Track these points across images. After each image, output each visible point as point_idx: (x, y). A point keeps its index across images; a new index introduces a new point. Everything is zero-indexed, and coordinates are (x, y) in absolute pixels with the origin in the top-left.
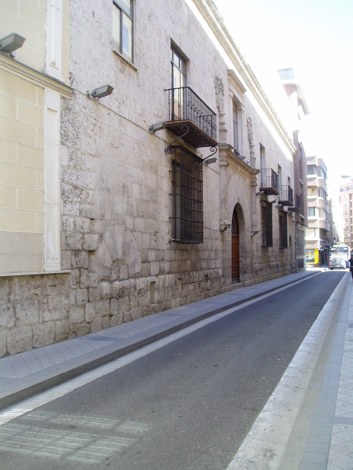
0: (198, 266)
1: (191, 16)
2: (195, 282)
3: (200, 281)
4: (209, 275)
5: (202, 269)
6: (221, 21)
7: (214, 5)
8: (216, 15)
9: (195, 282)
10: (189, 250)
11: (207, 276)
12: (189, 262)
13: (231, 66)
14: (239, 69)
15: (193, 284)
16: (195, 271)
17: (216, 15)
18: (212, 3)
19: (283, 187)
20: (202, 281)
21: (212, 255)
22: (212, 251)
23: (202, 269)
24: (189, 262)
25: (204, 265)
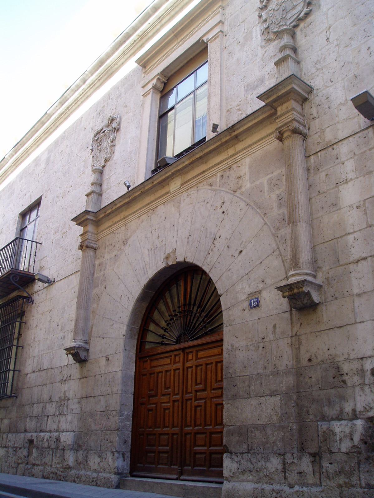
0: (21, 427)
1: (21, 177)
2: (8, 447)
3: (17, 447)
4: (35, 441)
5: (26, 431)
6: (87, 75)
7: (64, 93)
8: (78, 87)
9: (8, 447)
10: (8, 407)
11: (31, 442)
12: (6, 421)
13: (131, 65)
14: (14, 167)
15: (5, 449)
16: (14, 432)
17: (78, 87)
18: (63, 97)
19: (25, 242)
20: (20, 448)
21: (51, 409)
22: (52, 401)
23: (26, 431)
24: (6, 421)
25: (31, 424)
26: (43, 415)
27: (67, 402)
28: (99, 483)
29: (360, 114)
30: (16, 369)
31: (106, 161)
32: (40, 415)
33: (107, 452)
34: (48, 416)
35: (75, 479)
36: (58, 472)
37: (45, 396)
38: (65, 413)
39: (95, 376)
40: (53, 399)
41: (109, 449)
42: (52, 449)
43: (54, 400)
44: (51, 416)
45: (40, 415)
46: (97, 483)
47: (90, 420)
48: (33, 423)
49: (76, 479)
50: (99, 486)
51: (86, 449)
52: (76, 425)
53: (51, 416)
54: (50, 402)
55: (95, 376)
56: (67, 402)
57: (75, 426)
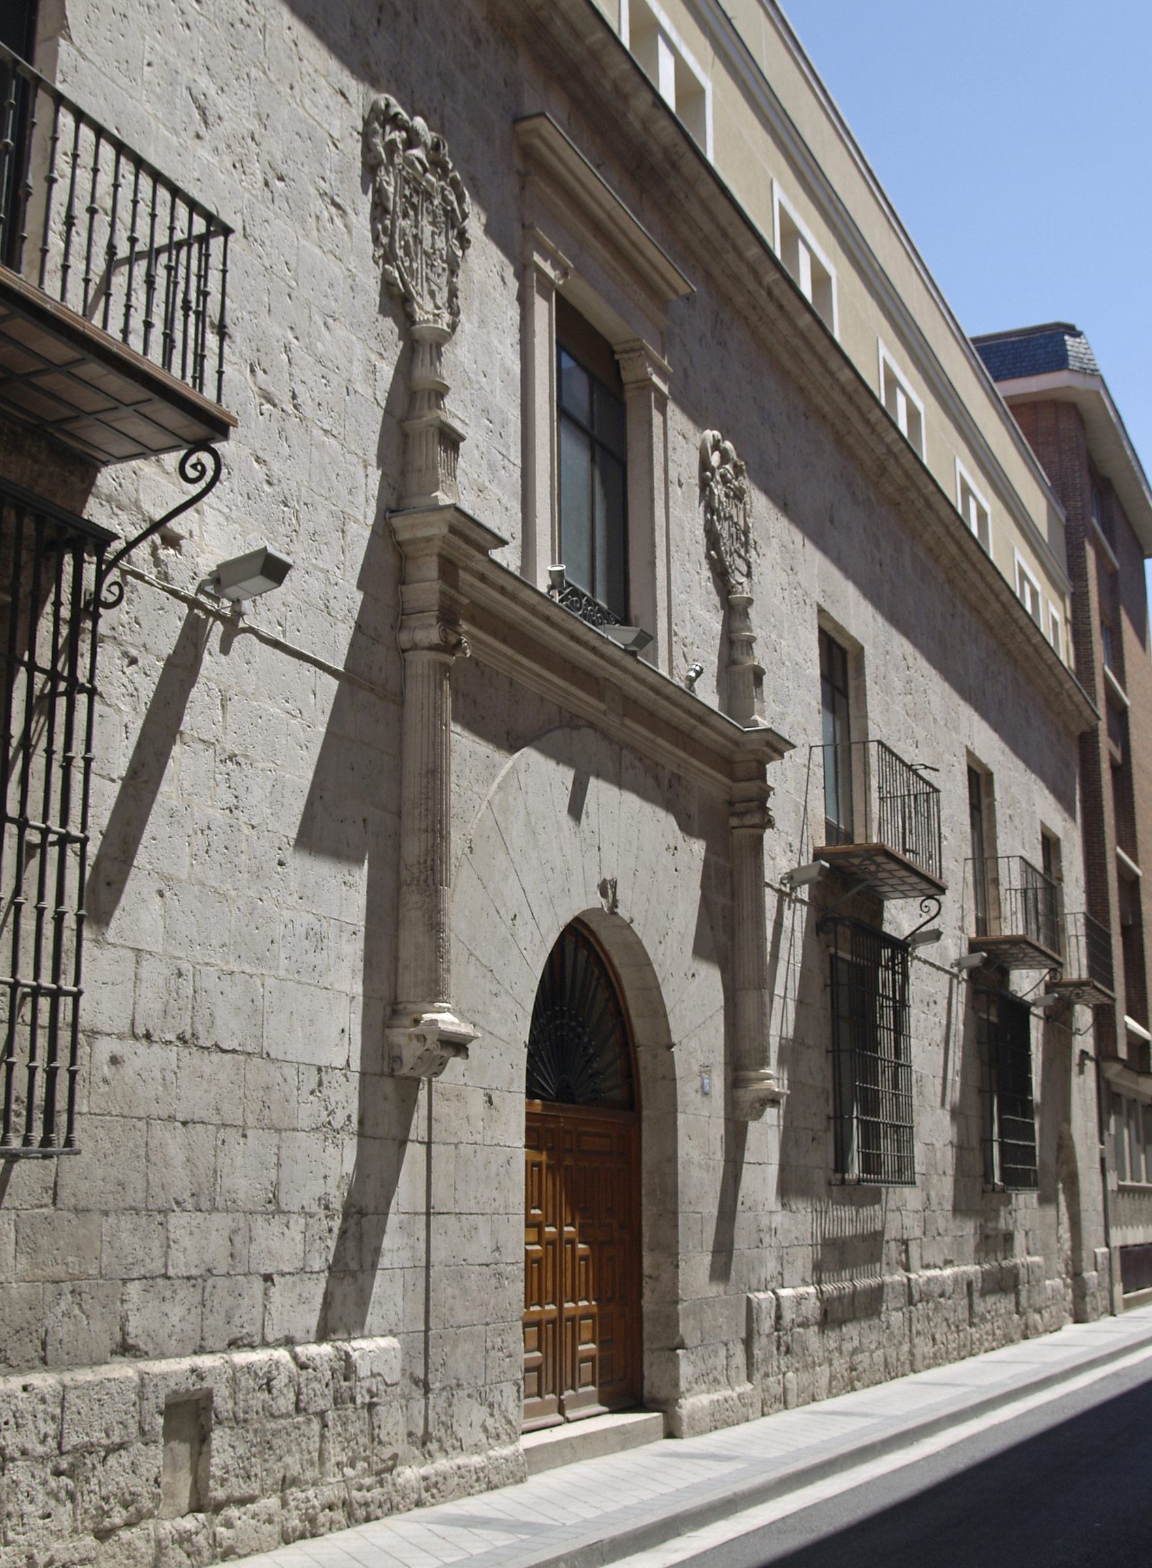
26: (240, 1269)
27: (358, 1224)
28: (495, 1479)
29: (378, 435)
30: (424, 1217)
31: (926, 767)
32: (222, 1269)
33: (503, 1386)
34: (268, 1278)
35: (420, 1495)
36: (355, 1493)
37: (243, 1182)
38: (354, 1266)
39: (456, 1145)
40: (289, 1201)
41: (508, 1376)
42: (316, 1414)
43: (296, 1209)
44: (283, 1275)
45: (222, 1269)
46: (489, 1482)
47: (449, 1291)
48: (176, 1312)
49: (424, 1495)
50: (496, 1487)
51: (444, 1389)
52: (400, 1312)
53: (283, 1275)
54: (273, 1214)
55: (456, 1145)
56: (358, 1224)
57: (397, 1314)
